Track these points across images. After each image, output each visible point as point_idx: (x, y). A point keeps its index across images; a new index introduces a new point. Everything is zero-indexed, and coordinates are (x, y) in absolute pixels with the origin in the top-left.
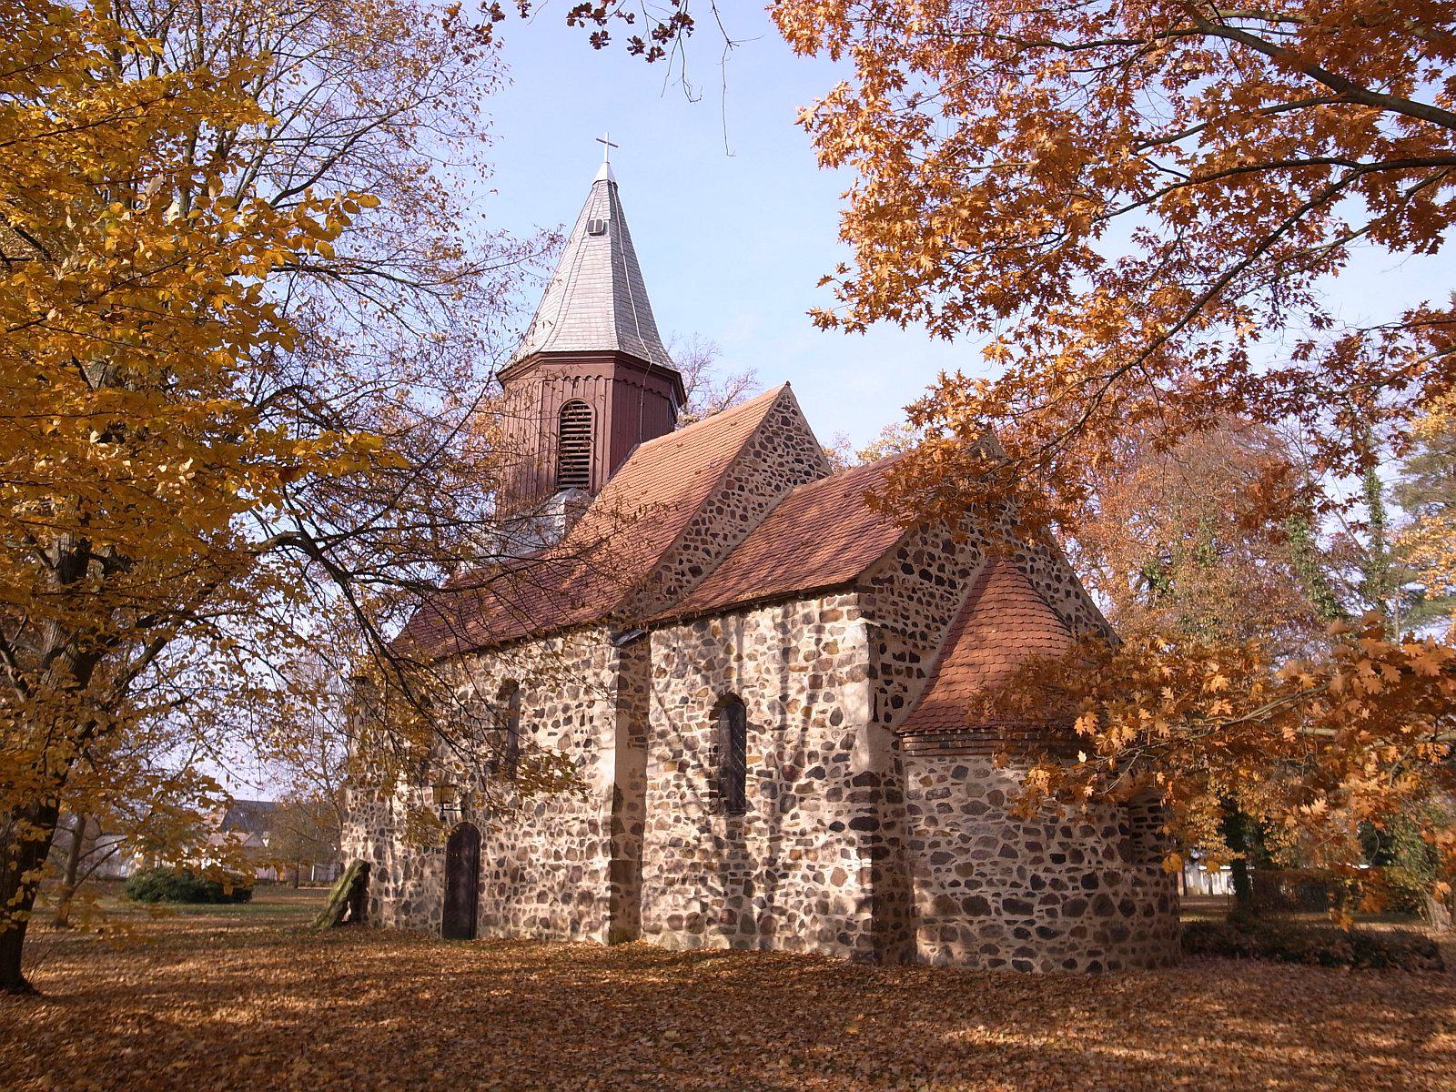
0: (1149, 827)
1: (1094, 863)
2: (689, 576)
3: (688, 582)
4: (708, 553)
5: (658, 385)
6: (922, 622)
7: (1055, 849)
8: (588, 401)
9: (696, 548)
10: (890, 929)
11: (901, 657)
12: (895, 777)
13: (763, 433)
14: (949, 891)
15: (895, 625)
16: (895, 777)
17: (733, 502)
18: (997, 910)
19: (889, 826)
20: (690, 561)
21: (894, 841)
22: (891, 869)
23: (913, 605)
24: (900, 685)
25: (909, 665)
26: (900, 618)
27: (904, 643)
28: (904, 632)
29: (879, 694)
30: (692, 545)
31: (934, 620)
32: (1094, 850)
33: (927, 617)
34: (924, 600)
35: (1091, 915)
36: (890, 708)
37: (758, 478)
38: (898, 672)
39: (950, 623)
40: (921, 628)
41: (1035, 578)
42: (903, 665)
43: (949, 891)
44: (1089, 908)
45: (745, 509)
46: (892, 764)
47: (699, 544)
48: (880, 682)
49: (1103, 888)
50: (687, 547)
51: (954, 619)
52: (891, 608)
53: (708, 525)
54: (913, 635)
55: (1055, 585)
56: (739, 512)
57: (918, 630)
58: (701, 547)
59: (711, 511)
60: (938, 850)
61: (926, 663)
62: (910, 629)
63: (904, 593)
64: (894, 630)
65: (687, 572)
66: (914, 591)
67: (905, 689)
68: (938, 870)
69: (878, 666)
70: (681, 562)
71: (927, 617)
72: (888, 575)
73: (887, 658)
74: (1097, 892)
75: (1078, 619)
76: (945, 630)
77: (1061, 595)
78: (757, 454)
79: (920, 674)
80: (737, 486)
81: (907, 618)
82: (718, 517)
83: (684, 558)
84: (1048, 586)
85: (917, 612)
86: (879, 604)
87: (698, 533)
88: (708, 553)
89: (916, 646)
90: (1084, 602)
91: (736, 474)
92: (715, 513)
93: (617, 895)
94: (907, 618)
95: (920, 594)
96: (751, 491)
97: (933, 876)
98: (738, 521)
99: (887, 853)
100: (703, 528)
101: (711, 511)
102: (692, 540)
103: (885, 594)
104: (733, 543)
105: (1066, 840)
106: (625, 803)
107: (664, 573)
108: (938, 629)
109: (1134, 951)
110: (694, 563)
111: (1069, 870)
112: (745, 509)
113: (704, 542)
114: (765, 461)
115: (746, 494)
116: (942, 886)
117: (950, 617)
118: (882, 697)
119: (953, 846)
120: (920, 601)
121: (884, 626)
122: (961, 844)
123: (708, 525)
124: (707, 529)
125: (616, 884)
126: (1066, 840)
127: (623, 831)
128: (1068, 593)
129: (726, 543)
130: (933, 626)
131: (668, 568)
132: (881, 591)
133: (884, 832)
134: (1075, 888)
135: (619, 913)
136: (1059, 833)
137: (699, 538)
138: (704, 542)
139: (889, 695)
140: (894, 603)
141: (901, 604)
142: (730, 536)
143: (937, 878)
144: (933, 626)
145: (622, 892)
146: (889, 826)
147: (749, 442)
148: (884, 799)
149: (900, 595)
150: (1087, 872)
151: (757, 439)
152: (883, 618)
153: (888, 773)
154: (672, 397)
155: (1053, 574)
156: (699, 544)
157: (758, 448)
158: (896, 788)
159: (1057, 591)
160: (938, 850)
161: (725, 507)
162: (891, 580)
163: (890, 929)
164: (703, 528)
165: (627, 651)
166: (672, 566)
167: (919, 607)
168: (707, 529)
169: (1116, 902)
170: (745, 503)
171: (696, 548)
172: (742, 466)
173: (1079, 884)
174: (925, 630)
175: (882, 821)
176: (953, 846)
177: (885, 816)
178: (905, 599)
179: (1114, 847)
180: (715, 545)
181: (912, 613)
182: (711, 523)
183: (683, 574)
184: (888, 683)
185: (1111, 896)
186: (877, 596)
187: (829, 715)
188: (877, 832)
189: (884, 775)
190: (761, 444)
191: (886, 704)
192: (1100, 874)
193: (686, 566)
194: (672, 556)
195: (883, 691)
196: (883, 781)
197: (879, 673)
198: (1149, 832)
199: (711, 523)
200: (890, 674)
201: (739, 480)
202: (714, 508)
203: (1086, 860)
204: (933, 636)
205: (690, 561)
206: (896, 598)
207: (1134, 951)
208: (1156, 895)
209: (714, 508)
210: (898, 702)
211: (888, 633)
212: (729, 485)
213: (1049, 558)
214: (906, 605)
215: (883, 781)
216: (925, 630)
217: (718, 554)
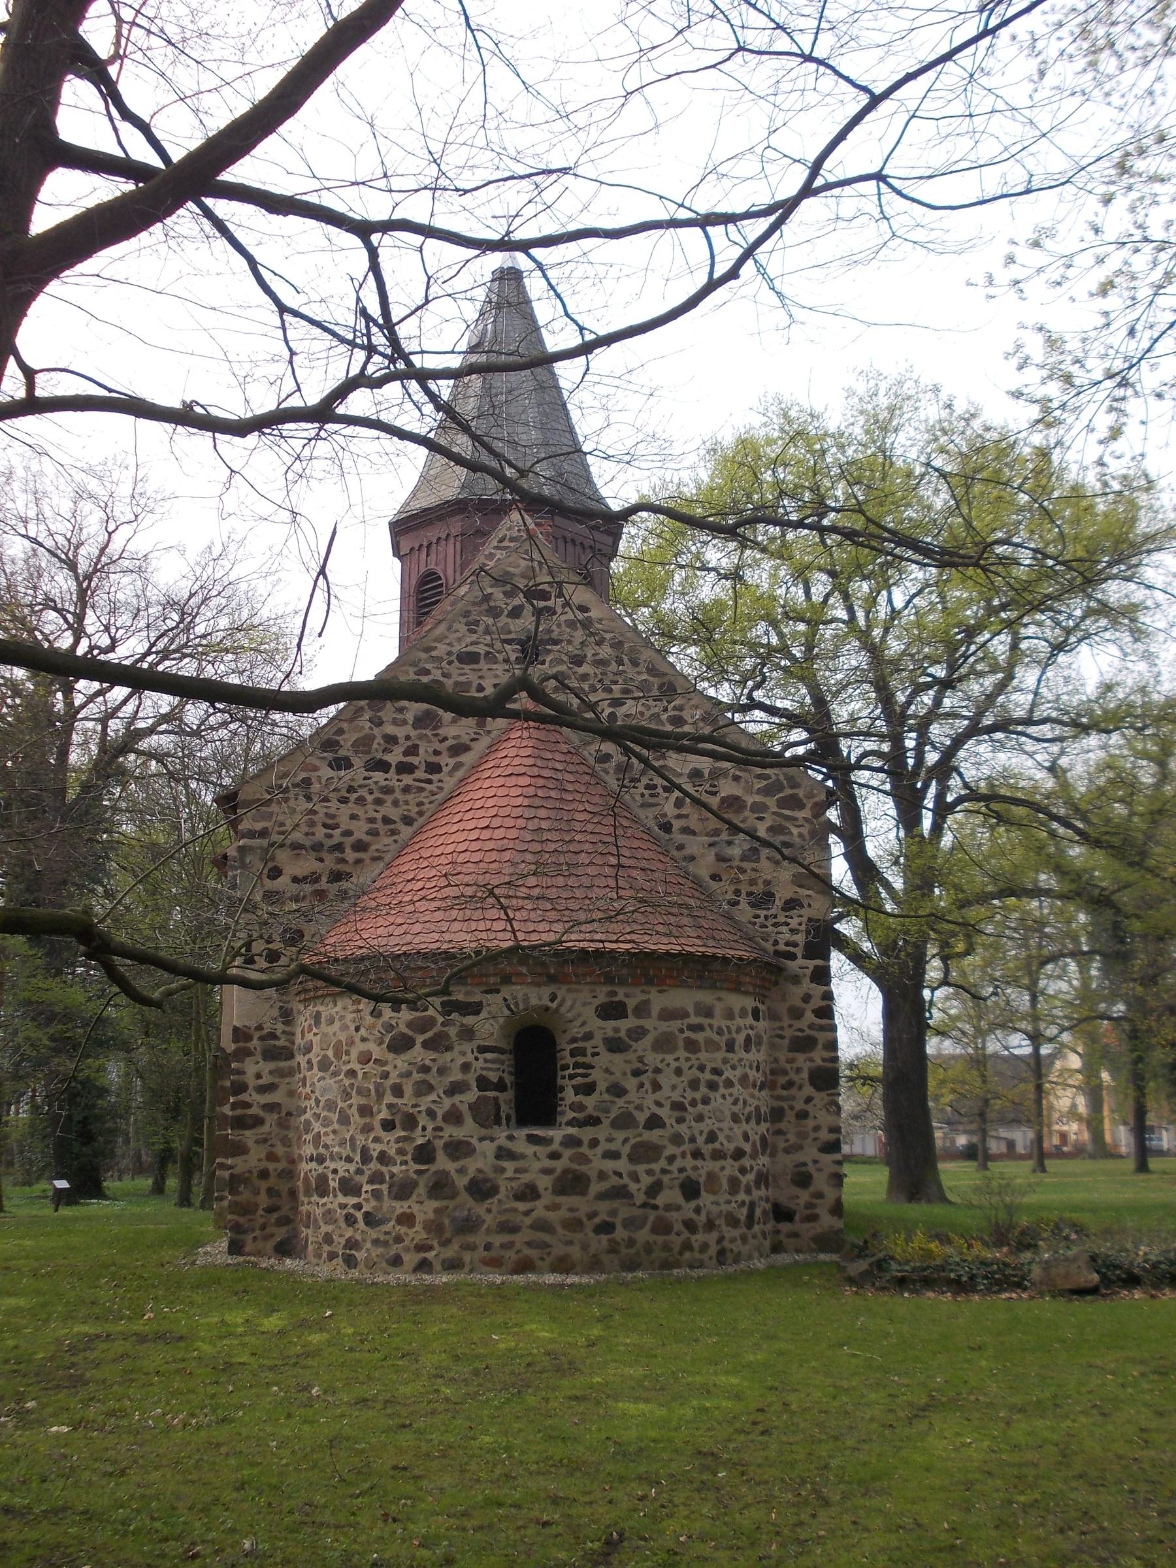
10: (260, 1212)
16: (280, 1028)
21: (271, 1107)
22: (265, 1141)
33: (372, 820)
44: (421, 1190)
49: (443, 1162)
54: (339, 847)
74: (433, 1168)
94: (336, 826)
133: (254, 1094)
158: (282, 1043)
167: (359, 811)
169: (461, 1182)
192: (439, 1144)
214: (332, 811)
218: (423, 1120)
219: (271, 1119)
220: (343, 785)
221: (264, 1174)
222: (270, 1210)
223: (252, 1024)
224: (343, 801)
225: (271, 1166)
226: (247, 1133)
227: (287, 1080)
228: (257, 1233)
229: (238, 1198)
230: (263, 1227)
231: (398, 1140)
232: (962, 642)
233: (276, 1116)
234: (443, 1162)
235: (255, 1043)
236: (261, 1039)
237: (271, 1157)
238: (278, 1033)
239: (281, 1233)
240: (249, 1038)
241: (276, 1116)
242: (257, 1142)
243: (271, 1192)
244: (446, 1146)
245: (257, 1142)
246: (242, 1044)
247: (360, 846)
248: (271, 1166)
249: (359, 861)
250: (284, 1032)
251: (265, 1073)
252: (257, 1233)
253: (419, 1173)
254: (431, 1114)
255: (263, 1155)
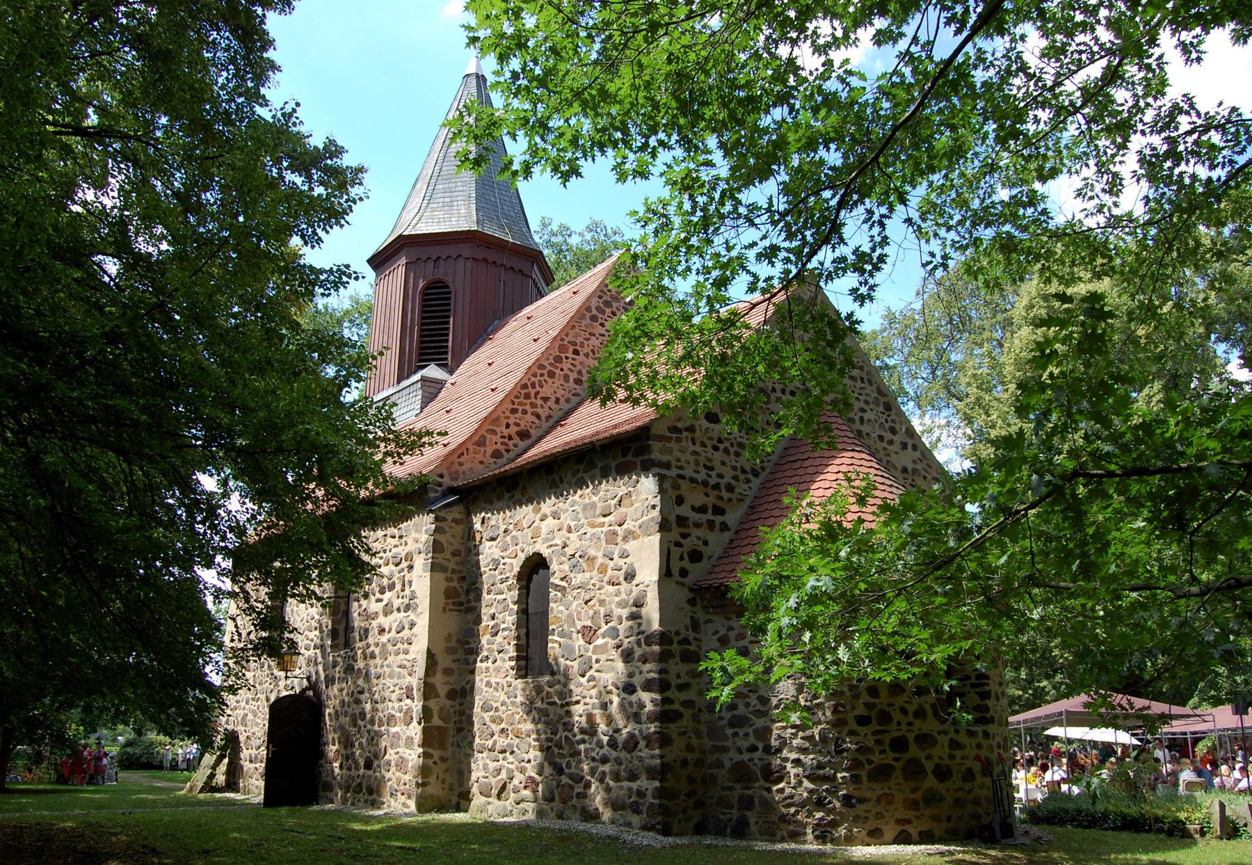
0: (973, 686)
1: (904, 724)
2: (517, 440)
3: (516, 446)
4: (538, 416)
5: (518, 264)
6: (728, 474)
7: (861, 710)
8: (449, 280)
9: (525, 412)
10: (682, 797)
11: (702, 509)
12: (691, 635)
13: (600, 297)
14: (746, 756)
15: (695, 475)
16: (691, 635)
17: (566, 365)
18: (896, 760)
19: (683, 687)
20: (518, 425)
21: (688, 704)
22: (685, 733)
23: (718, 456)
24: (698, 538)
25: (712, 518)
26: (701, 468)
27: (707, 495)
28: (705, 484)
29: (673, 548)
30: (520, 409)
31: (743, 471)
32: (904, 711)
33: (734, 468)
34: (732, 450)
35: (901, 780)
36: (686, 563)
37: (594, 342)
38: (697, 525)
39: (763, 475)
40: (728, 479)
41: (865, 428)
42: (703, 518)
43: (746, 756)
44: (898, 772)
45: (580, 372)
46: (688, 621)
47: (528, 408)
48: (675, 535)
49: (914, 751)
50: (514, 411)
51: (767, 471)
52: (692, 458)
53: (538, 388)
54: (716, 487)
55: (888, 436)
56: (573, 376)
57: (723, 482)
58: (530, 410)
59: (542, 375)
60: (735, 713)
61: (732, 517)
62: (713, 481)
63: (708, 443)
64: (692, 480)
65: (514, 435)
66: (720, 441)
67: (706, 543)
68: (736, 734)
69: (673, 518)
70: (508, 426)
71: (734, 468)
72: (688, 424)
73: (684, 510)
74: (906, 756)
75: (915, 470)
76: (756, 482)
77: (896, 447)
78: (594, 319)
79: (725, 527)
80: (571, 350)
81: (712, 469)
82: (550, 381)
83: (511, 421)
84: (881, 438)
85: (723, 463)
86: (676, 454)
87: (527, 396)
88: (538, 416)
89: (720, 498)
90: (923, 454)
91: (570, 338)
92: (546, 377)
93: (430, 762)
94: (712, 469)
95: (727, 444)
96: (587, 355)
97: (731, 741)
98: (572, 384)
99: (679, 715)
100: (533, 392)
101: (542, 375)
102: (520, 404)
103: (683, 443)
104: (565, 407)
105: (872, 700)
106: (440, 668)
107: (489, 436)
108: (748, 481)
109: (949, 819)
110: (522, 426)
111: (875, 733)
112: (580, 372)
113: (533, 405)
114: (602, 325)
115: (581, 358)
116: (740, 751)
117: (763, 469)
118: (676, 552)
119: (751, 709)
120: (726, 451)
121: (682, 477)
122: (759, 707)
123: (538, 388)
124: (537, 393)
125: (430, 750)
126: (872, 700)
127: (437, 696)
128: (904, 446)
129: (558, 407)
130: (742, 477)
131: (494, 432)
132: (679, 440)
133: (676, 693)
134: (882, 752)
135: (432, 779)
136: (865, 693)
137: (528, 401)
138: (533, 405)
139: (686, 549)
140: (695, 453)
141: (703, 454)
142: (562, 400)
143: (734, 743)
144: (742, 477)
145: (436, 758)
146: (683, 687)
147: (586, 307)
148: (678, 659)
149: (703, 445)
150: (897, 734)
151: (594, 303)
152: (681, 468)
153: (683, 631)
154: (536, 274)
155: (887, 425)
156: (528, 408)
157: (594, 312)
158: (693, 648)
159: (891, 442)
160: (735, 713)
161: (558, 371)
162: (691, 429)
163: (682, 797)
164: (533, 392)
165: (442, 514)
166: (498, 430)
167: (726, 459)
168: (537, 393)
169: (929, 766)
170: (579, 367)
171: (525, 412)
172: (577, 330)
173: (887, 748)
174: (733, 482)
175: (674, 682)
176: (751, 709)
177: (678, 676)
178: (710, 449)
179: (928, 708)
180: (546, 409)
181: (716, 464)
182: (541, 386)
183: (510, 438)
184: (685, 536)
185: (923, 761)
186: (673, 445)
187: (623, 572)
188: (668, 694)
189: (677, 633)
190: (598, 308)
191: (681, 558)
192: (911, 737)
193: (513, 429)
194: (497, 419)
195: (678, 544)
196: (676, 639)
197: (674, 525)
198: (973, 691)
199: (541, 386)
200: (686, 526)
201: (574, 344)
202: (545, 372)
203: (895, 722)
204: (741, 488)
205: (518, 425)
206: (698, 448)
207: (949, 819)
208: (977, 758)
209: (545, 372)
210: (696, 556)
211: (685, 485)
212: (562, 348)
213: (881, 409)
214: (709, 455)
215: (676, 639)
216: (733, 482)
217: (548, 417)
218: (897, 716)
219: (687, 713)
220: (715, 436)
221: (685, 763)
222: (689, 795)
223: (673, 629)
224: (716, 448)
225: (690, 756)
226: (672, 726)
227: (698, 680)
228: (681, 816)
229: (667, 785)
230: (684, 811)
231: (875, 733)
232: (19, 422)
233: (691, 712)
234: (914, 751)
235: (675, 647)
236: (680, 643)
237: (690, 748)
238: (691, 638)
239: (696, 816)
240: (671, 642)
241: (691, 712)
242: (679, 734)
243: (691, 780)
244: (917, 737)
245: (679, 734)
246: (666, 647)
247: (730, 488)
248: (690, 756)
249: (730, 500)
250: (695, 639)
251: (683, 674)
252: (681, 816)
253: (896, 760)
254: (904, 711)
255: (683, 746)
